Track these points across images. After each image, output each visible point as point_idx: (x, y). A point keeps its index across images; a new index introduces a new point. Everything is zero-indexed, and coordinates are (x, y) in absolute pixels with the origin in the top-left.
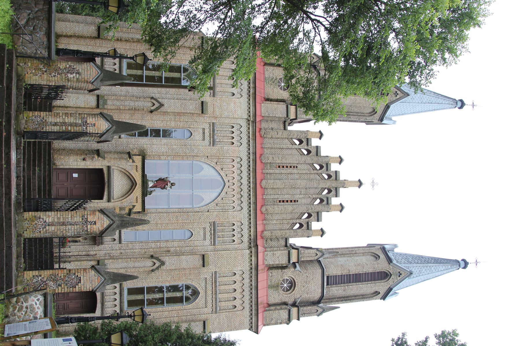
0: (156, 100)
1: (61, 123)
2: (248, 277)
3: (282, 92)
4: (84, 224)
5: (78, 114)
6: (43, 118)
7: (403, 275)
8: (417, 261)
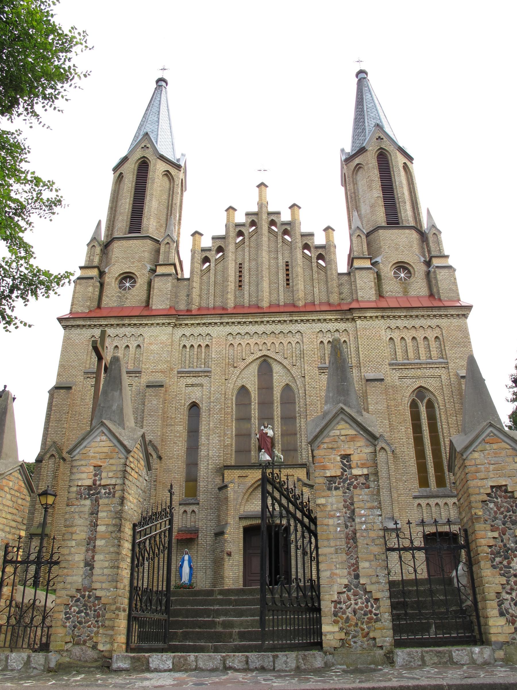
1: (87, 551)
2: (394, 321)
3: (137, 285)
4: (349, 484)
5: (68, 508)
6: (72, 597)
7: (380, 135)
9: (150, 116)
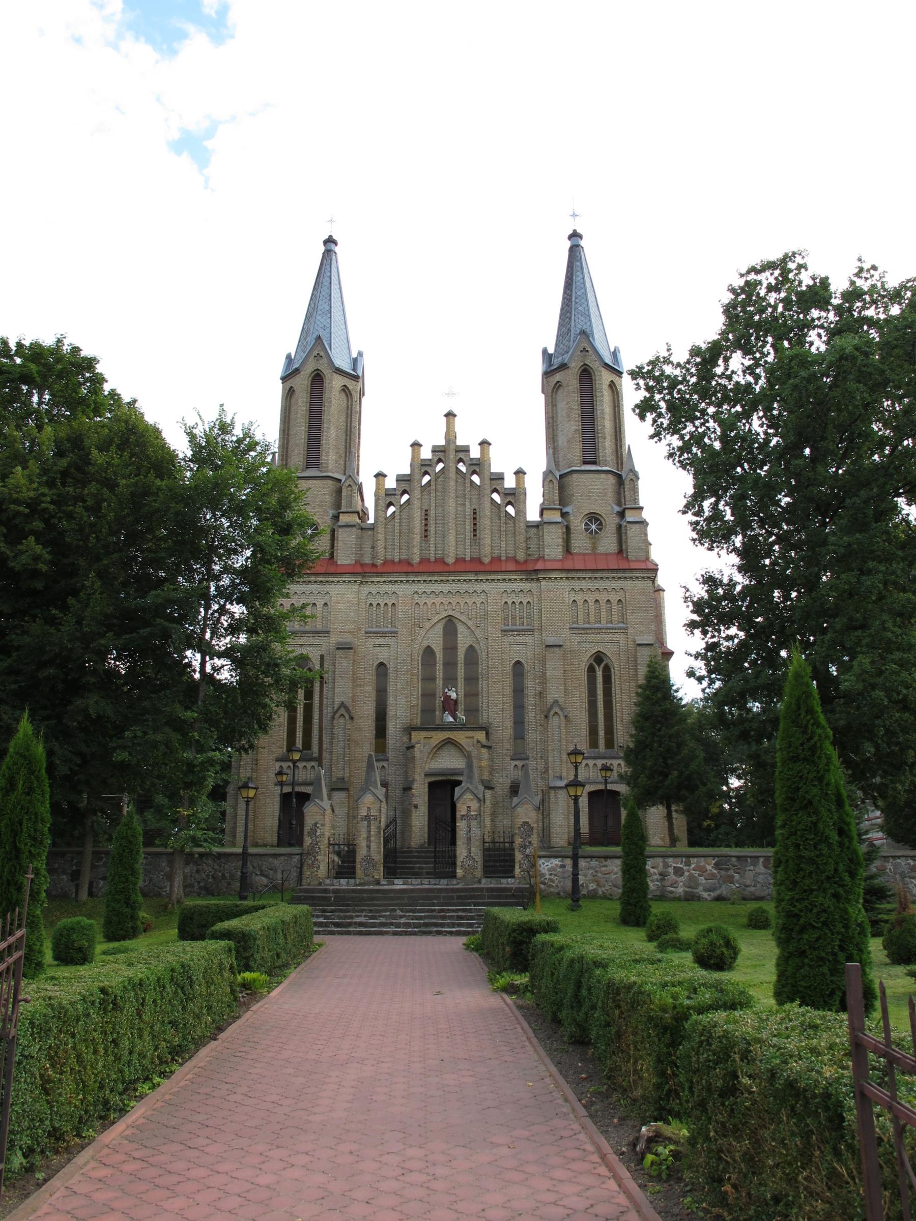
2: (578, 583)
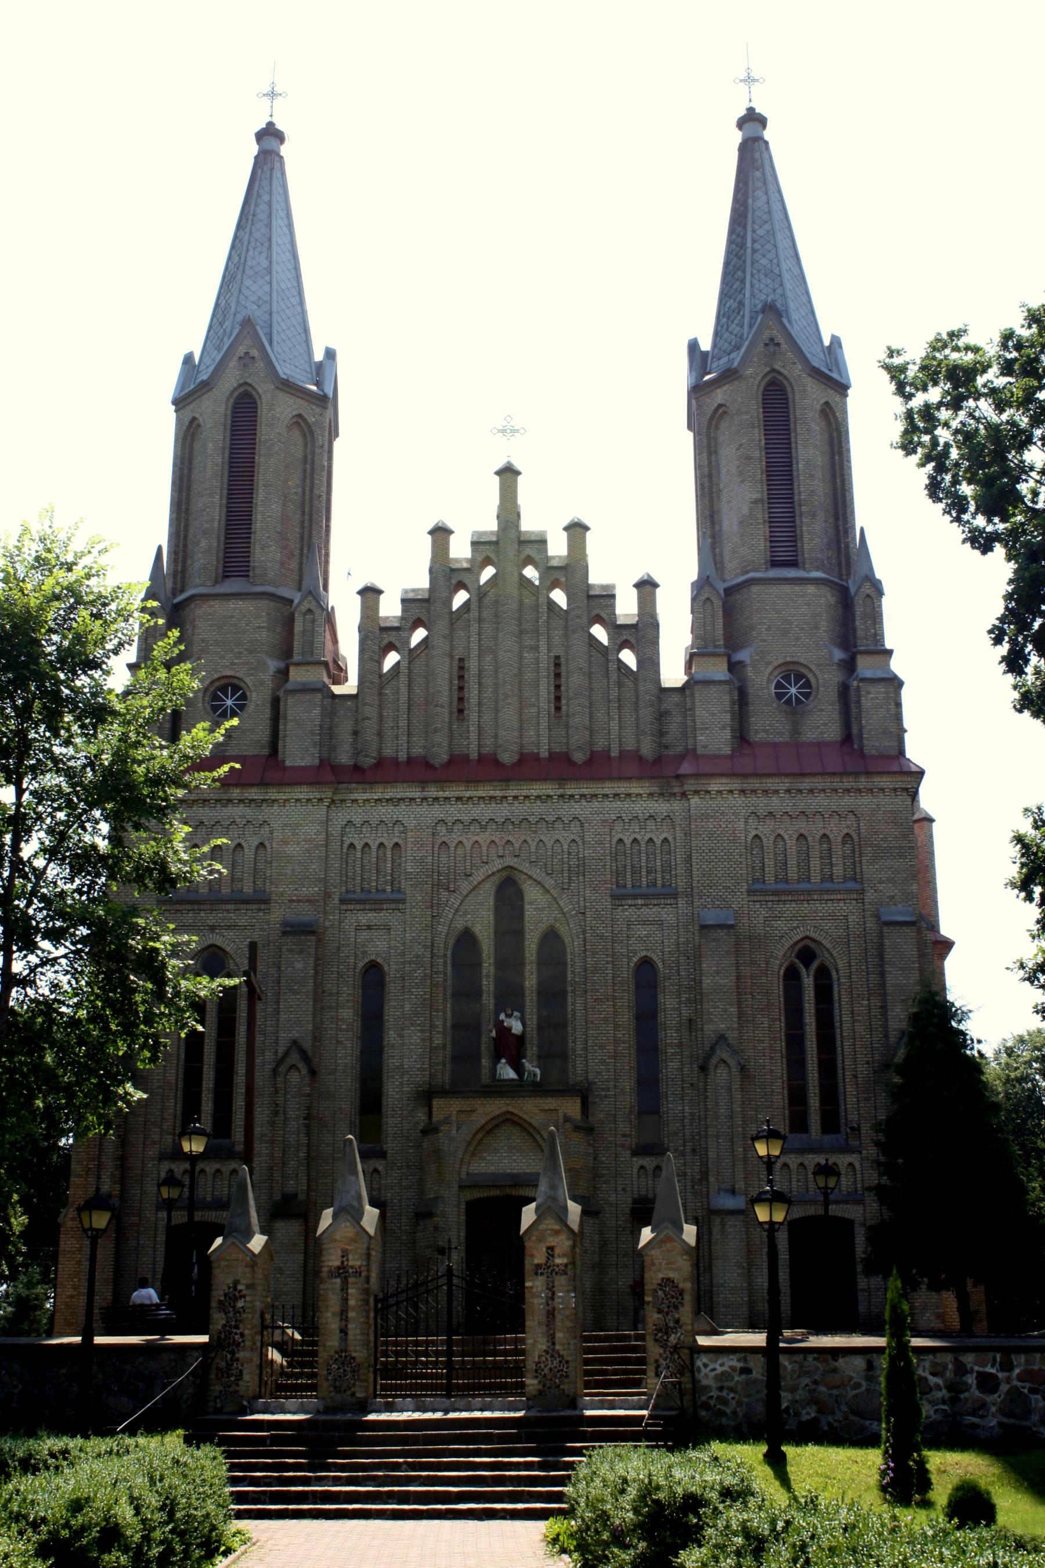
0: (280, 1062)
2: (764, 800)
8: (738, 283)
9: (251, 253)
